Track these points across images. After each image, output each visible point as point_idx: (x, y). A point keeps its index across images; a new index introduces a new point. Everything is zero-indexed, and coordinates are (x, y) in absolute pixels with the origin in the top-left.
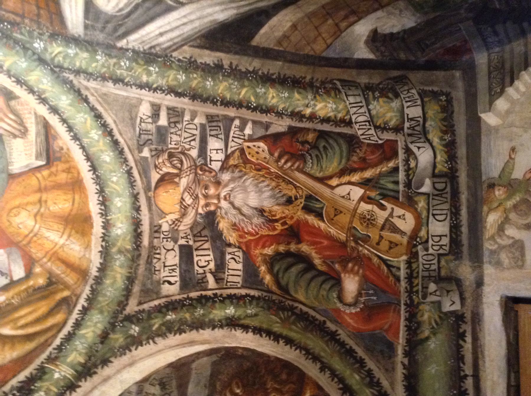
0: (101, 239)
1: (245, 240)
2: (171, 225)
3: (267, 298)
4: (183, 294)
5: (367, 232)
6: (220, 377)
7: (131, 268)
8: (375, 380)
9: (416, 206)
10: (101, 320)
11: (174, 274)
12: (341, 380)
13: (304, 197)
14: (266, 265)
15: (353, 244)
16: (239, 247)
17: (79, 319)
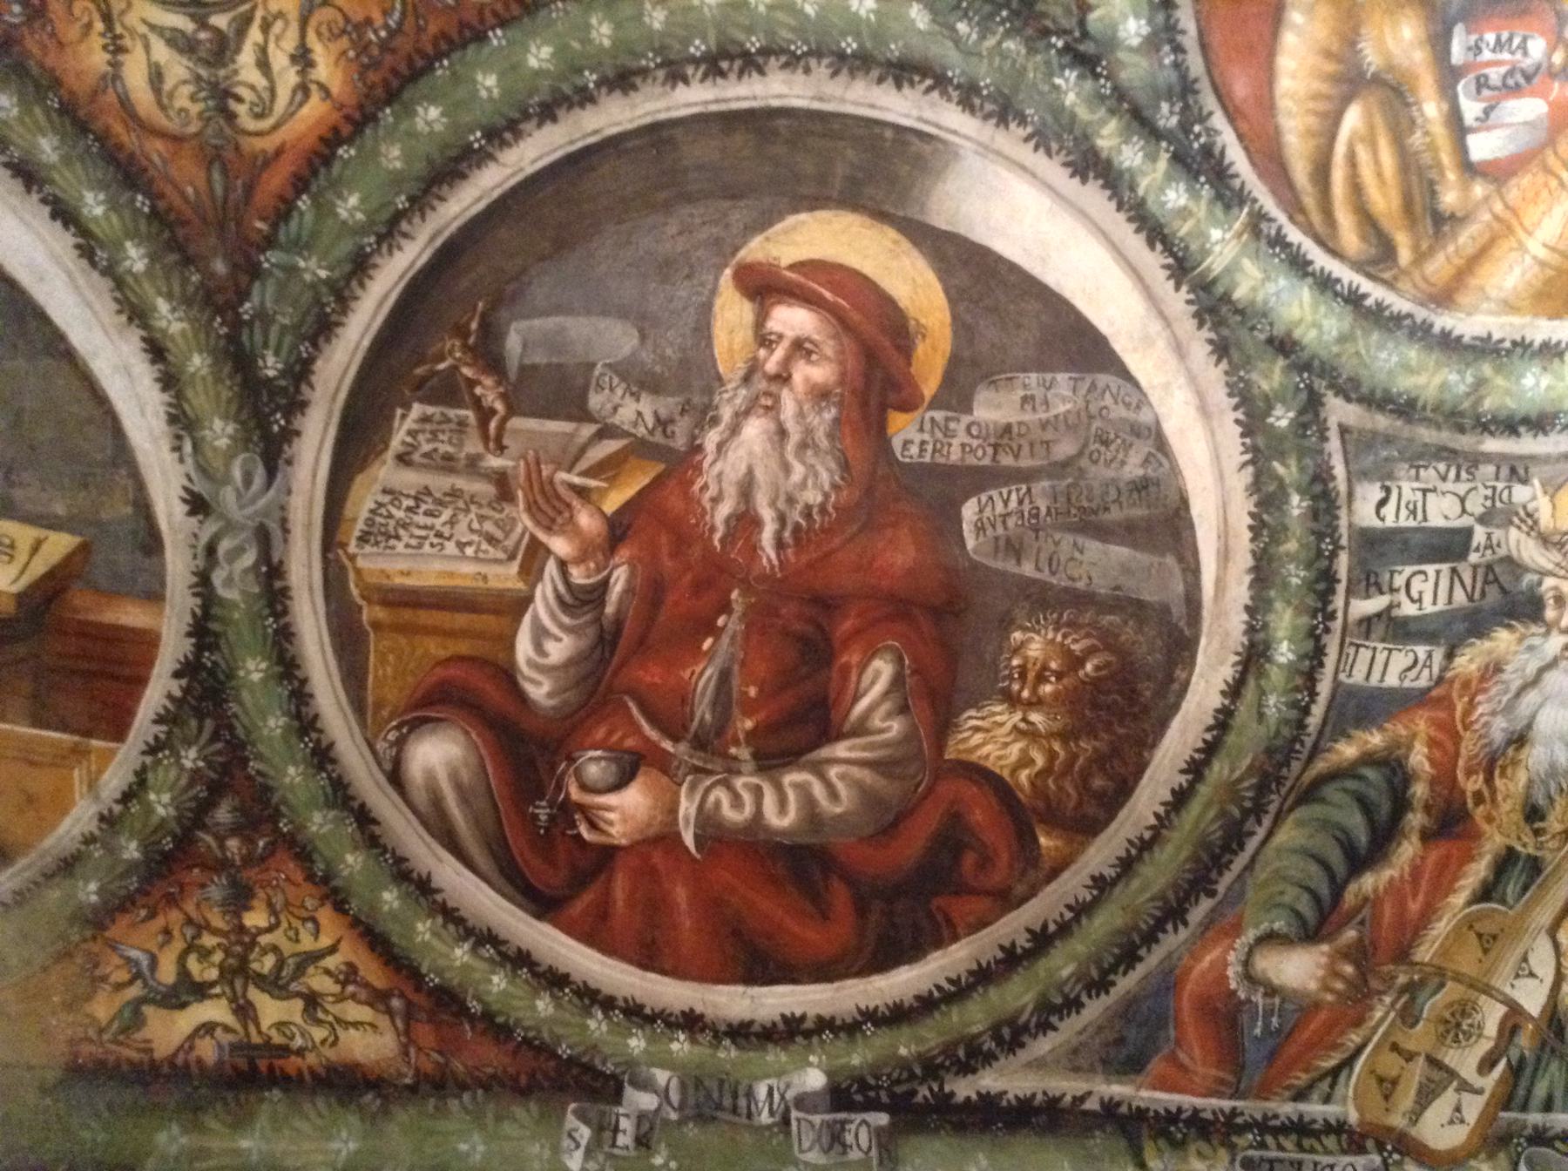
0: (1519, 339)
1: (1455, 695)
2: (1525, 507)
3: (1298, 747)
4: (1350, 537)
5: (1428, 1020)
6: (1131, 623)
7: (1433, 410)
8: (1054, 1019)
9: (1483, 1156)
10: (1325, 337)
11: (1404, 513)
12: (1064, 929)
13: (1539, 854)
14: (1385, 749)
15: (1402, 979)
16: (1440, 680)
17: (1338, 287)
